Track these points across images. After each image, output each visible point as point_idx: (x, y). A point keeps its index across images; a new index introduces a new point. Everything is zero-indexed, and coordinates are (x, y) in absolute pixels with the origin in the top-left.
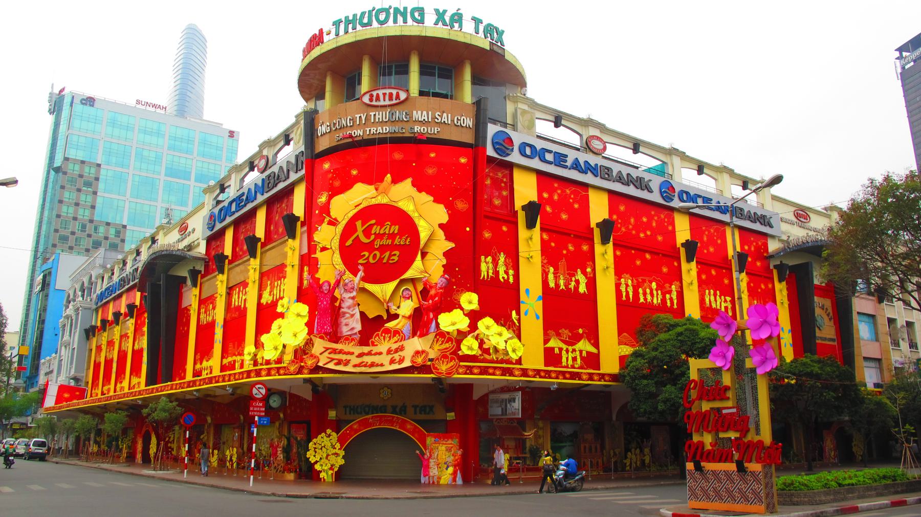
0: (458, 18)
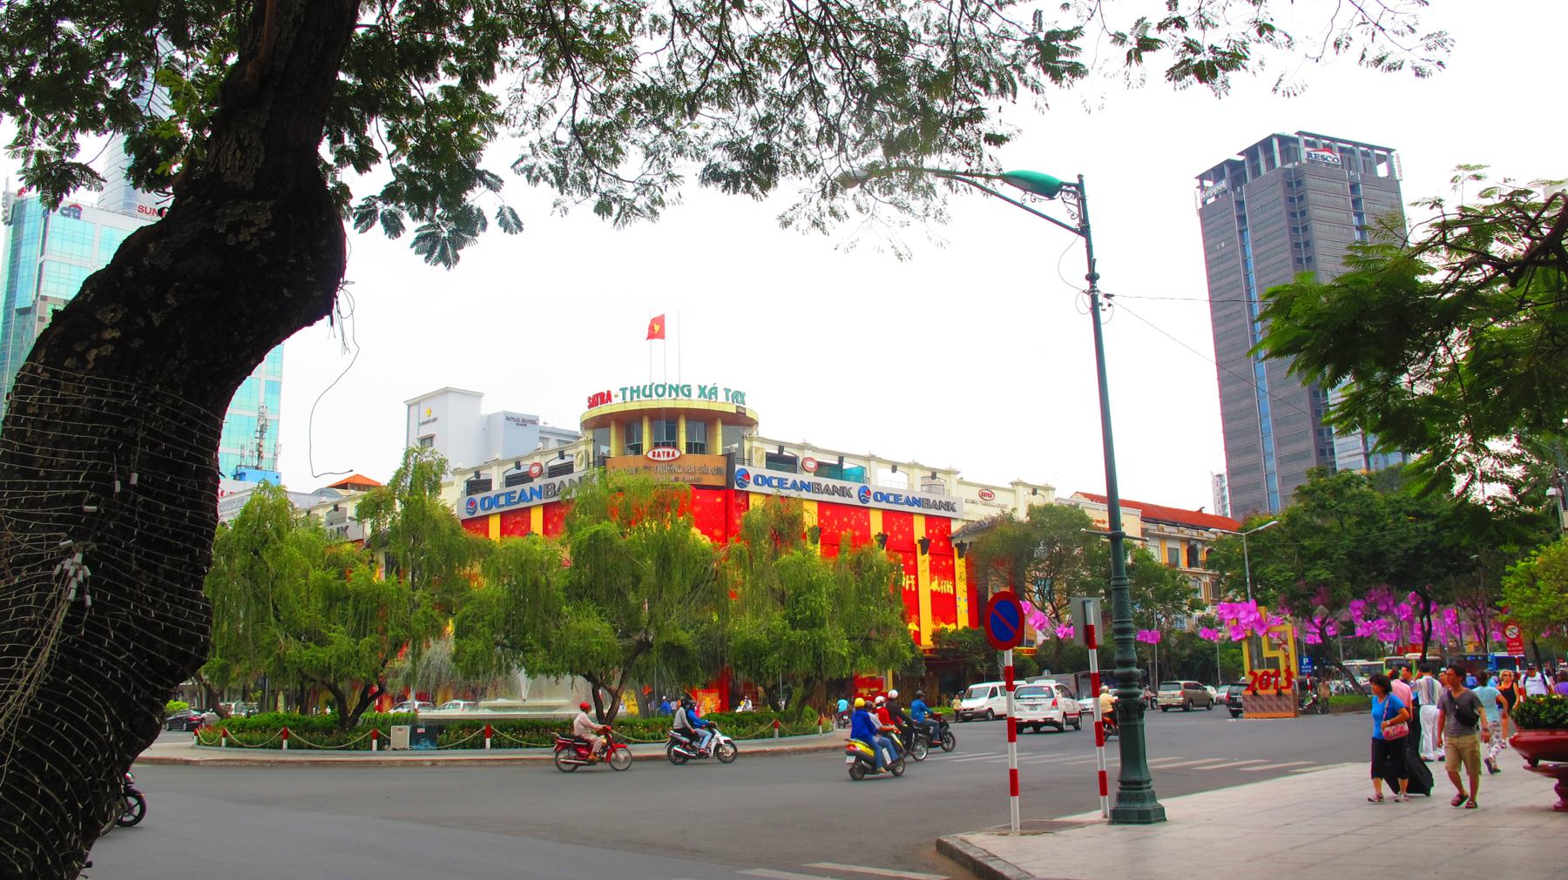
0: (714, 391)
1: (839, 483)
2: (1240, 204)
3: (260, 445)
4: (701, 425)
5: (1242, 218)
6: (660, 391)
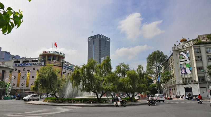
5: (93, 43)
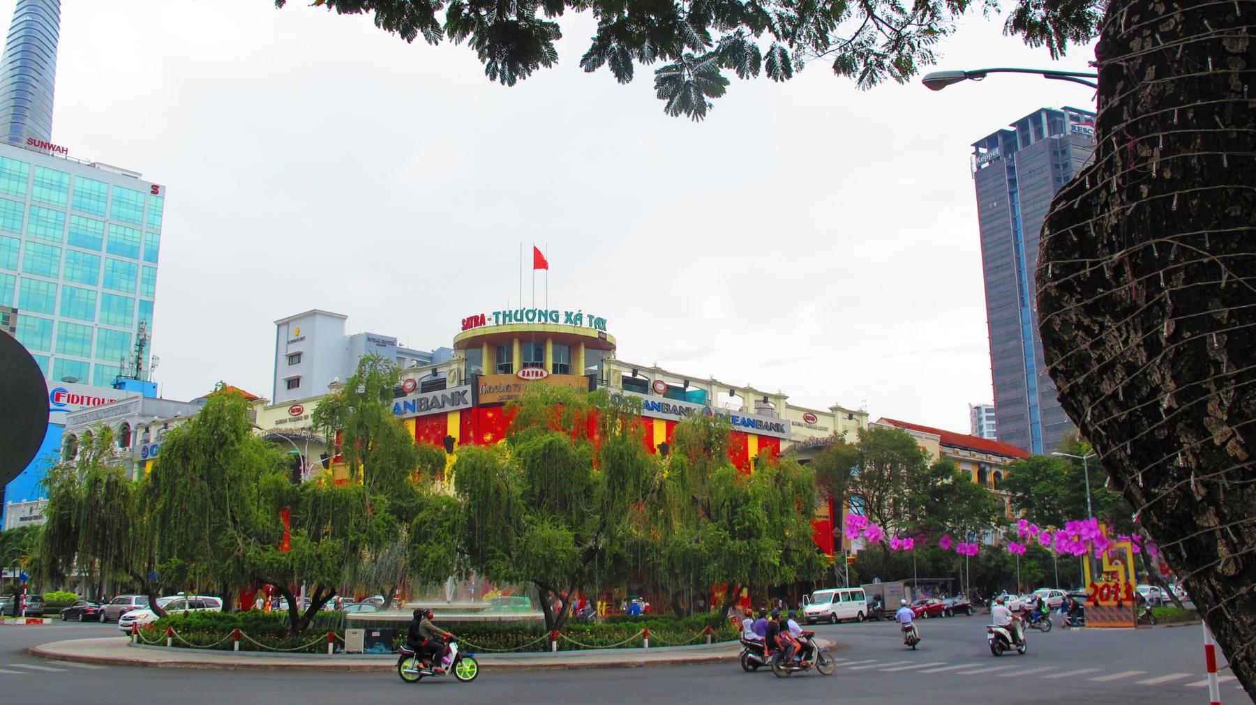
1: (685, 404)
2: (1011, 169)
3: (139, 358)
4: (566, 348)
5: (1012, 182)
6: (531, 316)
